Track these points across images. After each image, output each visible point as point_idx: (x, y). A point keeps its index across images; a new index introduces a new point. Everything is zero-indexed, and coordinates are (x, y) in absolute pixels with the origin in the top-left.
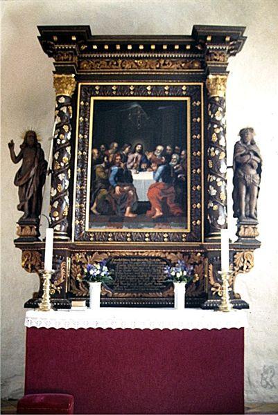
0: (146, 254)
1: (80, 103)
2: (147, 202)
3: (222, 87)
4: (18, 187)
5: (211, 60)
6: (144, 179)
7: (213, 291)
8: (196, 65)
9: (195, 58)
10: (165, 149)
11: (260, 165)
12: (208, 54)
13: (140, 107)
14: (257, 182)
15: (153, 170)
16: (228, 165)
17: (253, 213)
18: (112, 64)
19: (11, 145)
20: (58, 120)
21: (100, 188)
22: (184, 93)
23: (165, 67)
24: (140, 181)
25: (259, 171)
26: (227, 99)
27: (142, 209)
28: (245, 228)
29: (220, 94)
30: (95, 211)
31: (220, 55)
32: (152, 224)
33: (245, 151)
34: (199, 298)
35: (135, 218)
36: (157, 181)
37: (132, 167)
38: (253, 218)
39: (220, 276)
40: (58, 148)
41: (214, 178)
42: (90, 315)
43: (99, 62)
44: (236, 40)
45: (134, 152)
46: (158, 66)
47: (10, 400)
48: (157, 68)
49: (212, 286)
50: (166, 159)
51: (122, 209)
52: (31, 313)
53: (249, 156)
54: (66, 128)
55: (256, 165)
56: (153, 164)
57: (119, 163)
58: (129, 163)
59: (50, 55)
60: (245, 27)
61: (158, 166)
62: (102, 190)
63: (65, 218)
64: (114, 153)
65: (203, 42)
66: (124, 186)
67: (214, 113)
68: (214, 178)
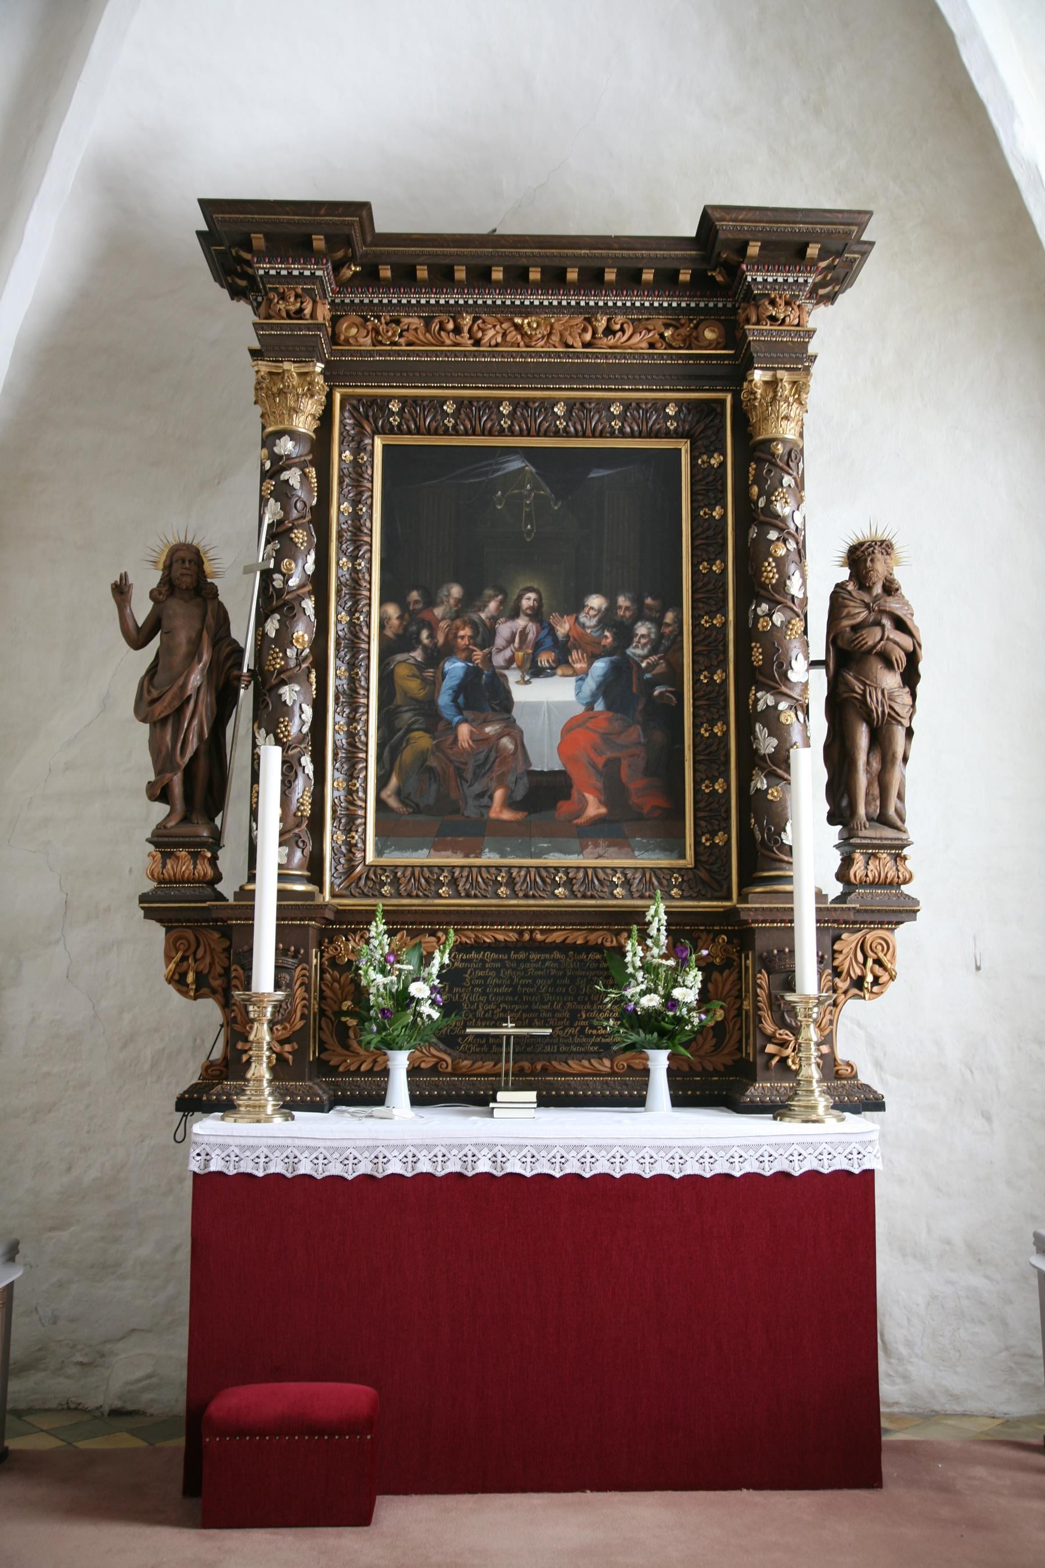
0: (557, 937)
1: (340, 456)
2: (560, 772)
3: (795, 408)
4: (146, 727)
5: (758, 323)
6: (549, 701)
7: (772, 1056)
8: (709, 335)
9: (706, 310)
10: (612, 606)
11: (913, 658)
12: (750, 298)
13: (530, 468)
14: (904, 711)
15: (575, 673)
16: (812, 658)
17: (891, 811)
18: (442, 328)
19: (121, 591)
20: (273, 511)
21: (410, 730)
22: (672, 425)
23: (611, 340)
24: (534, 708)
25: (911, 678)
26: (809, 446)
27: (545, 794)
28: (869, 857)
29: (788, 431)
30: (393, 803)
31: (788, 303)
32: (575, 843)
33: (864, 614)
34: (724, 1073)
35: (518, 822)
36: (590, 706)
37: (510, 661)
38: (898, 829)
39: (792, 1010)
40: (273, 601)
41: (770, 700)
42: (400, 1135)
43: (397, 322)
44: (839, 254)
45: (515, 614)
46: (588, 337)
47: (116, 1413)
48: (585, 345)
49: (770, 1039)
50: (615, 636)
51: (480, 795)
52: (207, 1127)
53: (877, 633)
54: (299, 536)
55: (899, 656)
56: (575, 655)
57: (467, 648)
58: (500, 651)
59: (236, 293)
60: (870, 213)
61: (593, 658)
62: (416, 734)
63: (304, 826)
64: (453, 620)
65: (735, 258)
66: (486, 722)
67: (769, 494)
68: (770, 700)
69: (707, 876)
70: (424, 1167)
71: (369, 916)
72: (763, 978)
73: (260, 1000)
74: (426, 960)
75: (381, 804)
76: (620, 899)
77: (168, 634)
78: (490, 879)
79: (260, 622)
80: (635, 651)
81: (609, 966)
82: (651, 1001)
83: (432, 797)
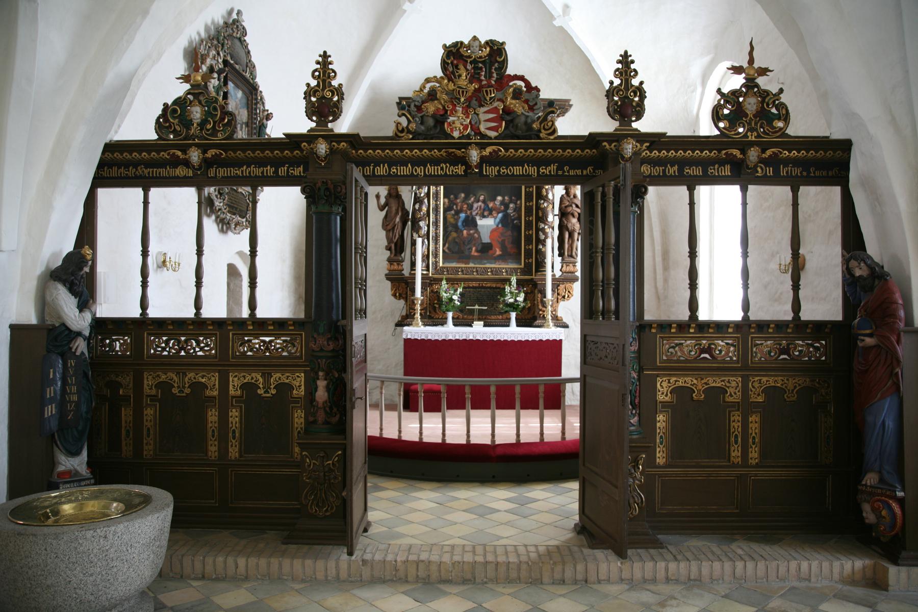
6: (487, 224)
10: (504, 199)
24: (483, 226)
27: (485, 249)
34: (529, 318)
42: (449, 331)
45: (478, 201)
61: (498, 213)
69: (527, 270)
70: (457, 338)
71: (441, 280)
72: (539, 295)
73: (417, 299)
74: (456, 290)
75: (444, 251)
76: (504, 275)
77: (390, 208)
78: (471, 271)
79: (414, 205)
80: (509, 211)
81: (502, 292)
82: (512, 300)
83: (457, 248)
